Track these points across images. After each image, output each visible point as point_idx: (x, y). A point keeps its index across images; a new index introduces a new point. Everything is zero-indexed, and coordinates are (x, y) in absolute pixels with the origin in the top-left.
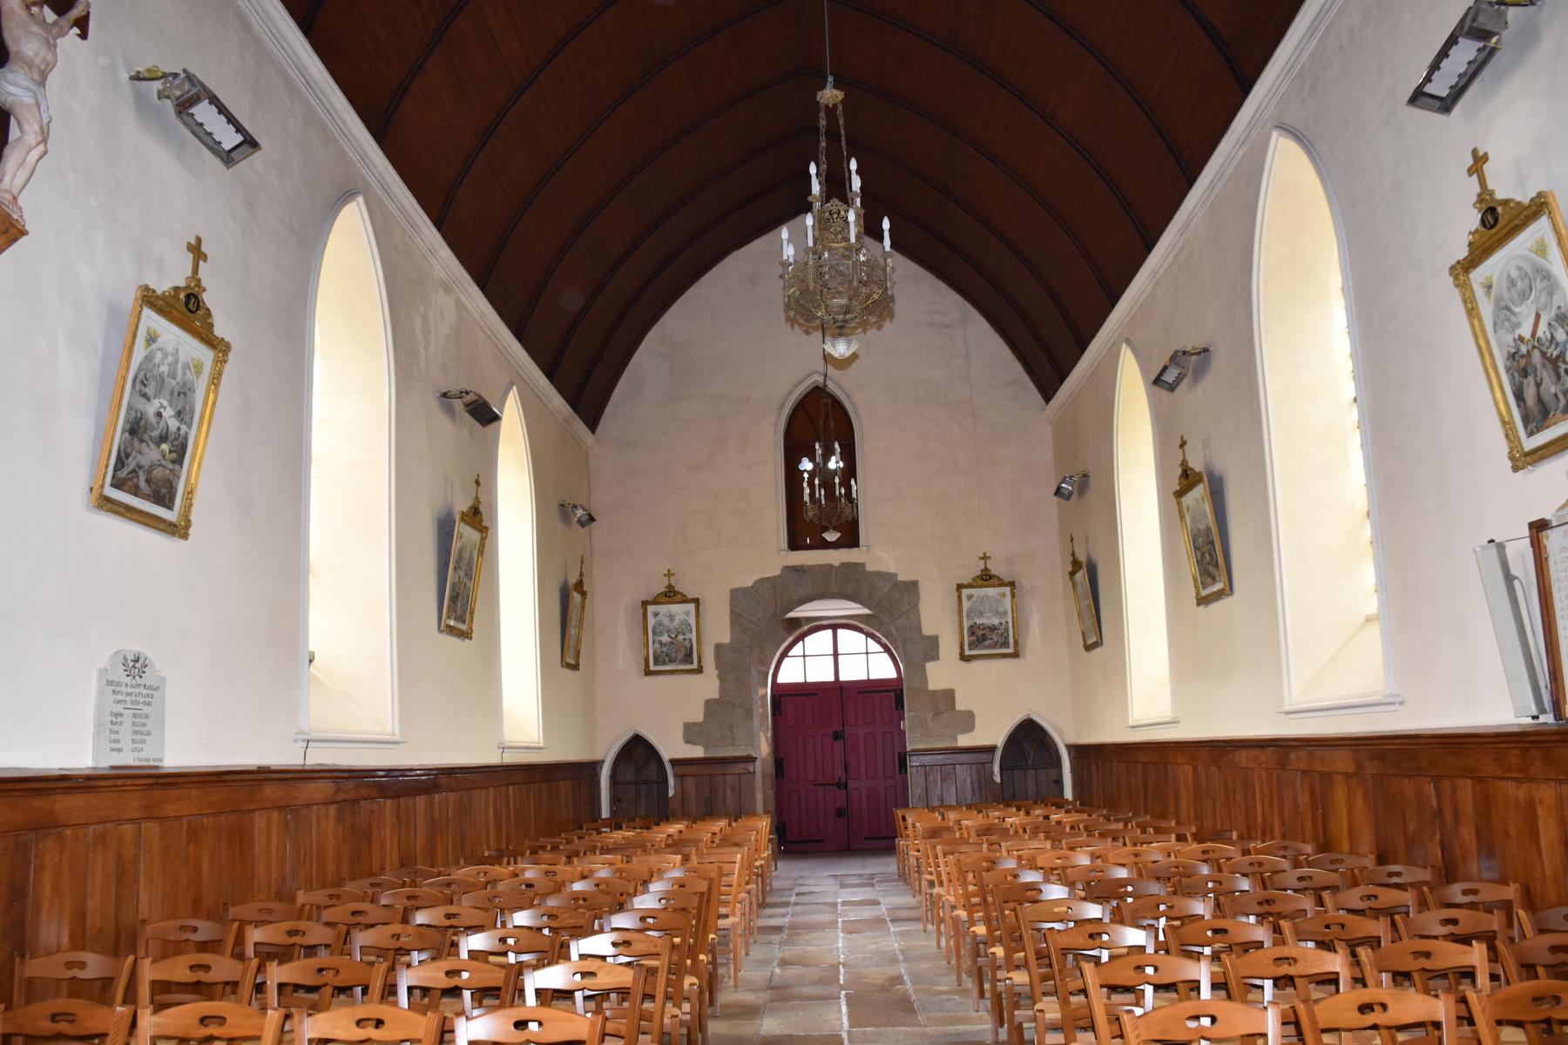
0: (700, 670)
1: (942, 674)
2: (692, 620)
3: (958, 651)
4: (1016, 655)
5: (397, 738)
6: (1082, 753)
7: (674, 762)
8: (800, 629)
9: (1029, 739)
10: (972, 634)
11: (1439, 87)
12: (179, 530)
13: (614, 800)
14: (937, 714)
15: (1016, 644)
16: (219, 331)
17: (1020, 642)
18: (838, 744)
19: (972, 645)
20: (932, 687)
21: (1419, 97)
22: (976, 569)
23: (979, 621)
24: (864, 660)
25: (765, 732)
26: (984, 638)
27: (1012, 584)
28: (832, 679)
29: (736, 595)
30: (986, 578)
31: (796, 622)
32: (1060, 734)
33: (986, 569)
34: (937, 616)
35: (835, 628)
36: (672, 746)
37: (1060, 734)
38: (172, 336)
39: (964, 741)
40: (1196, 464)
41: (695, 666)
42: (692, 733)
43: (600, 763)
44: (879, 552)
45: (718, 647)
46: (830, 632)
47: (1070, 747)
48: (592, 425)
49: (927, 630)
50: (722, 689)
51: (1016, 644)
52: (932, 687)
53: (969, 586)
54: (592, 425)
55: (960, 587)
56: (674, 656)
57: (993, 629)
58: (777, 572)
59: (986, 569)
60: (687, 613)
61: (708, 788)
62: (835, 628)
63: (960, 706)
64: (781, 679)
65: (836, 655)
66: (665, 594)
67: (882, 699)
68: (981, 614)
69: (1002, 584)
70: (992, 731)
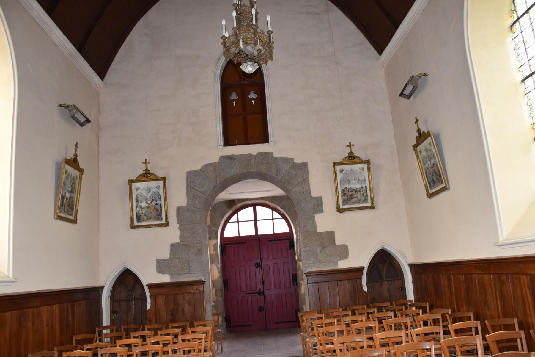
0: (167, 224)
1: (324, 222)
2: (161, 192)
4: (372, 207)
5: (13, 280)
6: (418, 269)
7: (150, 286)
8: (235, 206)
9: (384, 262)
10: (344, 194)
11: (407, 92)
12: (74, 221)
13: (113, 312)
14: (324, 248)
15: (372, 200)
16: (81, 167)
17: (375, 199)
18: (259, 270)
19: (345, 202)
20: (319, 230)
21: (401, 95)
23: (348, 186)
26: (352, 197)
27: (368, 162)
28: (253, 233)
29: (191, 176)
30: (351, 158)
31: (231, 203)
32: (405, 257)
33: (351, 152)
35: (254, 206)
36: (149, 276)
38: (69, 168)
39: (342, 265)
40: (423, 129)
41: (164, 221)
42: (162, 266)
43: (101, 288)
44: (282, 142)
45: (179, 209)
46: (251, 208)
47: (411, 266)
48: (102, 73)
50: (182, 237)
51: (372, 200)
52: (319, 230)
53: (341, 164)
54: (102, 73)
55: (335, 164)
56: (149, 216)
57: (356, 191)
58: (217, 160)
59: (351, 152)
60: (158, 187)
61: (175, 304)
62: (254, 206)
63: (338, 242)
64: (226, 235)
65: (255, 220)
66: (144, 175)
67: (284, 241)
68: (349, 181)
69: (361, 162)
70: (360, 258)
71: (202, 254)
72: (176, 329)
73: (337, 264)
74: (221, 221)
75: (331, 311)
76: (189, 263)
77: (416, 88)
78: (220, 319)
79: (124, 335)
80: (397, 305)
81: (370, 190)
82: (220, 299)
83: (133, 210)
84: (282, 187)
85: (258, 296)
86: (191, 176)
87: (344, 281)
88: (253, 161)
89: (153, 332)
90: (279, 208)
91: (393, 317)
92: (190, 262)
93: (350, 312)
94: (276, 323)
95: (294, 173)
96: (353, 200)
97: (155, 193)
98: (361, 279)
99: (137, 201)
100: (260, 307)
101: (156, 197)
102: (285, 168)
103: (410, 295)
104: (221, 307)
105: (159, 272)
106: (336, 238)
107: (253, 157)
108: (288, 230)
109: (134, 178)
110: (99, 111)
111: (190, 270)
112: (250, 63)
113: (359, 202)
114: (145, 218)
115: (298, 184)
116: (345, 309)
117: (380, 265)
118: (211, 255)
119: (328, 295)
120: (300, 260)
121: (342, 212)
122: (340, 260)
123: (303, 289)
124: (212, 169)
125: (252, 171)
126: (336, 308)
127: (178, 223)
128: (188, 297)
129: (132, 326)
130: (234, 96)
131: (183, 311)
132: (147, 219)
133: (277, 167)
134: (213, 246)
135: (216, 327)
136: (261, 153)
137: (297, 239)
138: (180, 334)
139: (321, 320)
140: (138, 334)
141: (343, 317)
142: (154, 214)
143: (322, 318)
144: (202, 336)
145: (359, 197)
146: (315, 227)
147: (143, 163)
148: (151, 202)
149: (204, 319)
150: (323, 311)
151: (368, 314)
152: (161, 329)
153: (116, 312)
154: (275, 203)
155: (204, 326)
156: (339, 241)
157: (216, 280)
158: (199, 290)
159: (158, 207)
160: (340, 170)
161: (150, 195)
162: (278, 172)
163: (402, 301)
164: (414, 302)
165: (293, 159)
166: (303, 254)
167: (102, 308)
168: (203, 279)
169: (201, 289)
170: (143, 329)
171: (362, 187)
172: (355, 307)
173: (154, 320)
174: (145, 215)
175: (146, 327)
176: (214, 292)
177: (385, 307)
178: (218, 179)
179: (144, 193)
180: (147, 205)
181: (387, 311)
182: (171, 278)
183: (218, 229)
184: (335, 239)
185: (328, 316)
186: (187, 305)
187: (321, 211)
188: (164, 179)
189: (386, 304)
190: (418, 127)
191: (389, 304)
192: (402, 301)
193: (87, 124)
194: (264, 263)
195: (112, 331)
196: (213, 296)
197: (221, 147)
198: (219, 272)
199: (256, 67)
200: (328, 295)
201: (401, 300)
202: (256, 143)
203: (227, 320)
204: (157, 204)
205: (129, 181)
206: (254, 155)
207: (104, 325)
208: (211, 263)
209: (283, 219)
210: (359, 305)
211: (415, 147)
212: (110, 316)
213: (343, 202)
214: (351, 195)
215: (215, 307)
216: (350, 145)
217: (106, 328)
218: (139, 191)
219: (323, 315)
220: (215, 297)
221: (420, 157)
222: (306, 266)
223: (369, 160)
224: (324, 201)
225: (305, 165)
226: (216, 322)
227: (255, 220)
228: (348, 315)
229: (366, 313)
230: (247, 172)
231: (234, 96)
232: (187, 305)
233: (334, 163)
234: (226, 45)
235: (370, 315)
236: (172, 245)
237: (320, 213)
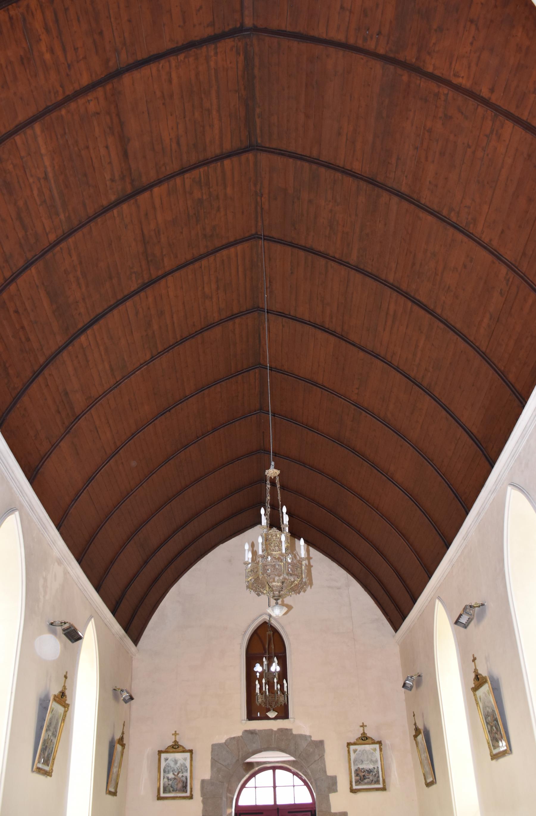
0: (191, 797)
2: (188, 764)
3: (349, 786)
4: (384, 789)
15: (384, 781)
17: (386, 781)
23: (361, 767)
30: (364, 739)
34: (336, 764)
35: (274, 768)
41: (188, 794)
45: (203, 781)
46: (271, 771)
49: (330, 773)
51: (384, 781)
53: (355, 744)
55: (349, 744)
57: (369, 771)
60: (185, 759)
64: (241, 803)
69: (374, 743)
81: (382, 771)
86: (216, 748)
88: (273, 736)
96: (366, 781)
99: (164, 772)
108: (309, 800)
114: (171, 789)
115: (315, 761)
132: (173, 791)
133: (295, 744)
136: (281, 729)
146: (329, 806)
147: (173, 734)
148: (178, 774)
154: (297, 769)
160: (354, 750)
174: (171, 787)
178: (240, 753)
179: (172, 764)
180: (173, 776)
183: (234, 795)
187: (335, 791)
188: (191, 751)
213: (356, 782)
214: (364, 776)
216: (363, 726)
225: (321, 742)
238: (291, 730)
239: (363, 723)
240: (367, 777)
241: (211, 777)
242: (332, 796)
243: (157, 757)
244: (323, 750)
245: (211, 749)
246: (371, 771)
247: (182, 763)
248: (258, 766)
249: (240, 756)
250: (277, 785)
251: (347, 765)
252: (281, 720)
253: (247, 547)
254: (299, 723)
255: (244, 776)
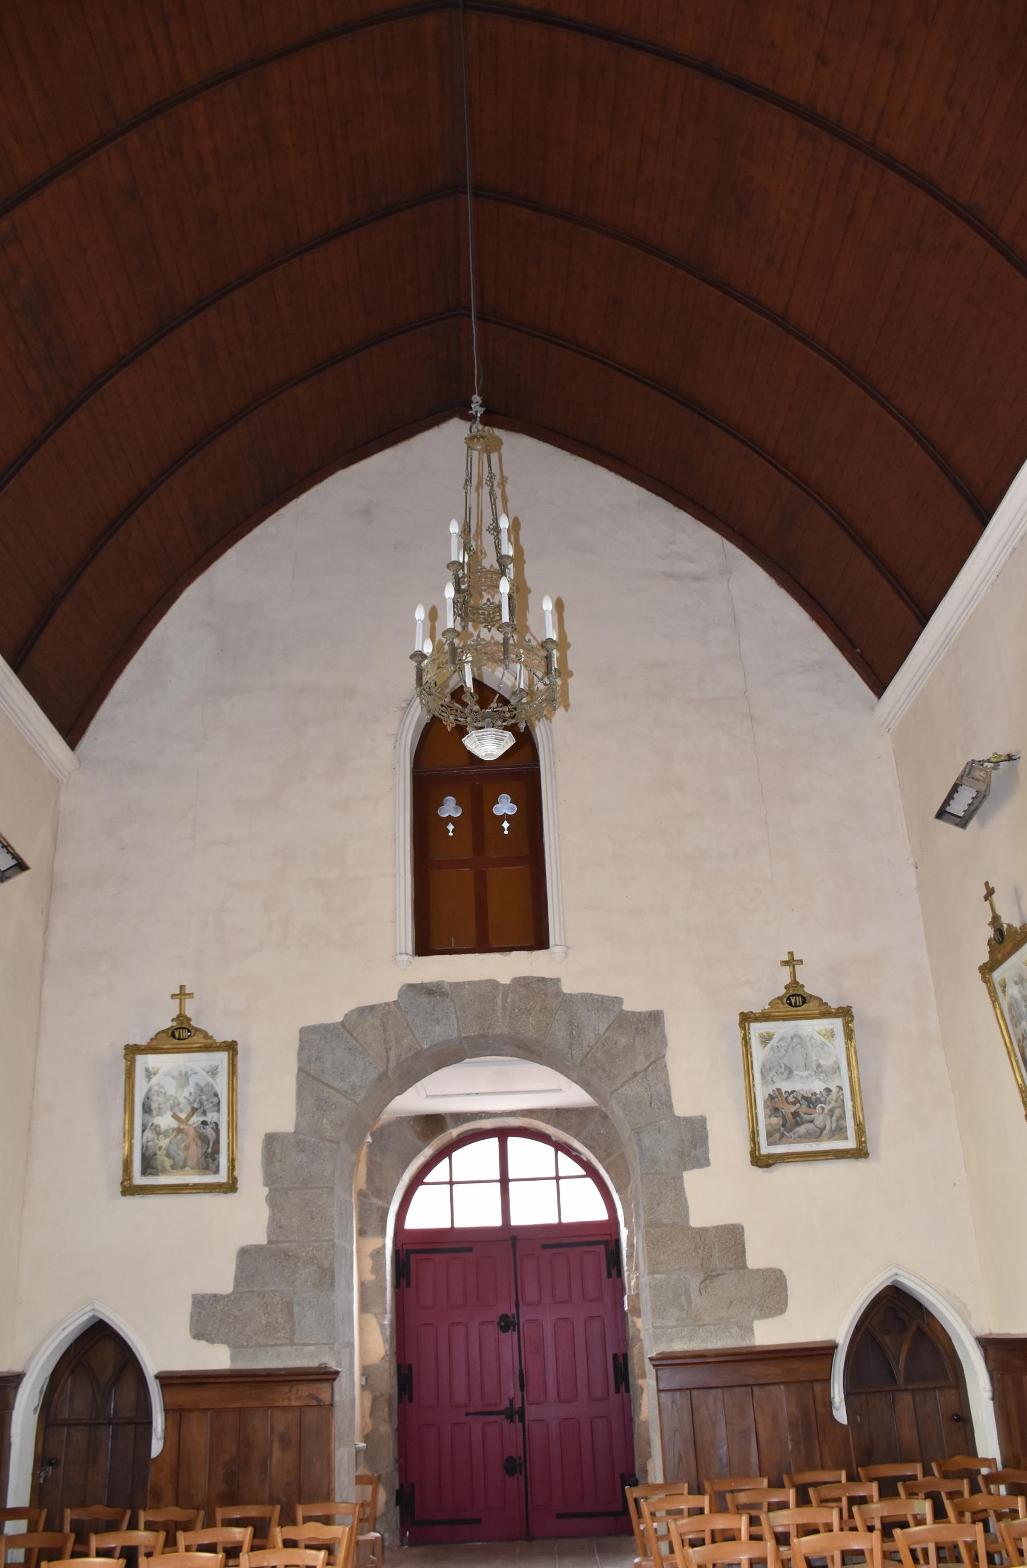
0: (231, 1187)
1: (714, 1194)
2: (221, 1085)
3: (747, 1147)
4: (860, 1153)
7: (168, 1381)
8: (441, 1134)
11: (958, 807)
13: (43, 1459)
14: (709, 1276)
15: (860, 1130)
17: (868, 1128)
18: (509, 1338)
20: (696, 1220)
22: (778, 984)
23: (786, 1087)
24: (551, 1193)
25: (379, 1316)
27: (845, 1013)
28: (497, 1222)
29: (314, 1041)
30: (796, 1001)
31: (432, 1123)
33: (795, 983)
34: (703, 1080)
35: (502, 1134)
36: (167, 1347)
37: (964, 1315)
39: (768, 1333)
40: (1010, 918)
41: (222, 1177)
42: (208, 1316)
45: (271, 1140)
46: (494, 1142)
48: (72, 727)
49: (683, 1107)
50: (275, 1226)
51: (860, 1130)
52: (696, 1220)
53: (764, 1017)
54: (72, 727)
55: (746, 1019)
57: (811, 1101)
58: (392, 996)
60: (213, 1072)
62: (502, 1134)
63: (755, 1259)
64: (412, 1223)
65: (504, 1181)
66: (172, 1033)
67: (599, 1243)
69: (826, 1013)
70: (823, 1315)
71: (332, 1285)
72: (237, 1530)
73: (752, 1330)
74: (399, 1177)
75: (733, 1486)
76: (291, 1313)
77: (984, 797)
78: (382, 1496)
79: (70, 1545)
80: (945, 1475)
81: (853, 1099)
82: (387, 1430)
83: (132, 1138)
84: (586, 1085)
85: (506, 1423)
86: (314, 1041)
87: (772, 1388)
88: (499, 1001)
89: (162, 1535)
90: (577, 1144)
91: (929, 1518)
92: (296, 1309)
93: (791, 1495)
94: (560, 1516)
95: (623, 1041)
96: (802, 1130)
97: (201, 1089)
98: (827, 1381)
99: (147, 1109)
100: (510, 1459)
101: (204, 1101)
102: (596, 1025)
103: (988, 1441)
104: (388, 1452)
105: (197, 1336)
106: (747, 1246)
107: (501, 990)
108: (600, 1214)
109: (143, 1042)
110: (55, 839)
111: (293, 1333)
112: (490, 731)
113: (817, 1135)
114: (168, 1163)
115: (635, 1075)
116: (776, 1484)
117: (887, 1339)
118: (362, 1285)
119: (724, 1434)
120: (637, 1311)
121: (768, 1166)
122: (762, 1318)
123: (648, 1405)
124: (377, 1022)
125: (497, 1031)
126: (747, 1475)
127: (266, 1184)
128: (282, 1422)
129: (100, 1511)
130: (450, 808)
131: (264, 1466)
132: (173, 1167)
133: (571, 1023)
134: (372, 1256)
135: (366, 1520)
136: (524, 978)
137: (631, 1245)
138: (246, 1547)
139: (696, 1518)
140: (114, 1540)
141: (770, 1510)
142: (195, 1152)
143: (701, 1511)
144: (317, 1558)
145: (819, 1120)
146: (682, 1209)
147: (173, 996)
148: (188, 1118)
149: (327, 1496)
150: (707, 1485)
151: (853, 1501)
152: (187, 1526)
153: (53, 1462)
154: (566, 1130)
155: (327, 1520)
156: (758, 1256)
157: (375, 1367)
158: (319, 1400)
159: (209, 1131)
160: (761, 1036)
161: (186, 1094)
162: (573, 1037)
163: (960, 1461)
164: (1000, 1466)
165: (618, 1001)
166: (646, 1295)
167: (9, 1445)
168: (333, 1366)
169: (325, 1396)
170: (133, 1526)
171: (828, 1090)
172: (809, 1477)
173: (169, 1495)
174: (168, 1155)
175: (143, 1517)
176: (368, 1404)
177: (905, 1479)
178: (392, 1054)
179: (170, 1087)
180: (175, 1124)
181: (911, 1494)
182: (233, 1358)
183: (389, 1202)
184: (744, 1252)
185: (720, 1506)
186: (276, 1446)
187: (702, 1161)
188: (231, 1047)
189: (906, 1470)
190: (993, 911)
191: (918, 1469)
192: (960, 1461)
193: (16, 874)
194: (525, 1315)
195: (32, 1528)
196: (363, 1417)
197: (405, 958)
198: (385, 1341)
199: (509, 741)
200: (722, 1431)
201: (958, 1458)
202: (510, 949)
203: (405, 1498)
204: (204, 1123)
205: (127, 1047)
206: (504, 985)
207: (11, 1503)
208: (364, 1308)
209: (589, 1180)
210: (823, 1468)
211: (987, 970)
212: (34, 1474)
213: (769, 1135)
214: (795, 1114)
215: (368, 1456)
216: (791, 962)
217: (16, 1513)
218: (154, 1080)
219: (706, 1499)
220: (368, 1420)
221: (1004, 1002)
222: (656, 1332)
223: (849, 1008)
224: (712, 1128)
225: (655, 1018)
226: (369, 1504)
227: (504, 1181)
228: (784, 1506)
229: (844, 1500)
230: (481, 1036)
231: (450, 808)
232: (276, 1446)
233: (742, 1014)
234: (424, 681)
235: (855, 1509)
236: (245, 1253)
237: (701, 1166)
238: (557, 981)
239: (791, 953)
240: (807, 1117)
241: (297, 1126)
242: (692, 1179)
243: (122, 1064)
244: (662, 1041)
245: (298, 1043)
246: (818, 1101)
247: (202, 1084)
248: (456, 1126)
249: (391, 1066)
250: (511, 1175)
251: (741, 1083)
252: (525, 953)
253: (420, 614)
254: (579, 956)
255: (418, 1151)
